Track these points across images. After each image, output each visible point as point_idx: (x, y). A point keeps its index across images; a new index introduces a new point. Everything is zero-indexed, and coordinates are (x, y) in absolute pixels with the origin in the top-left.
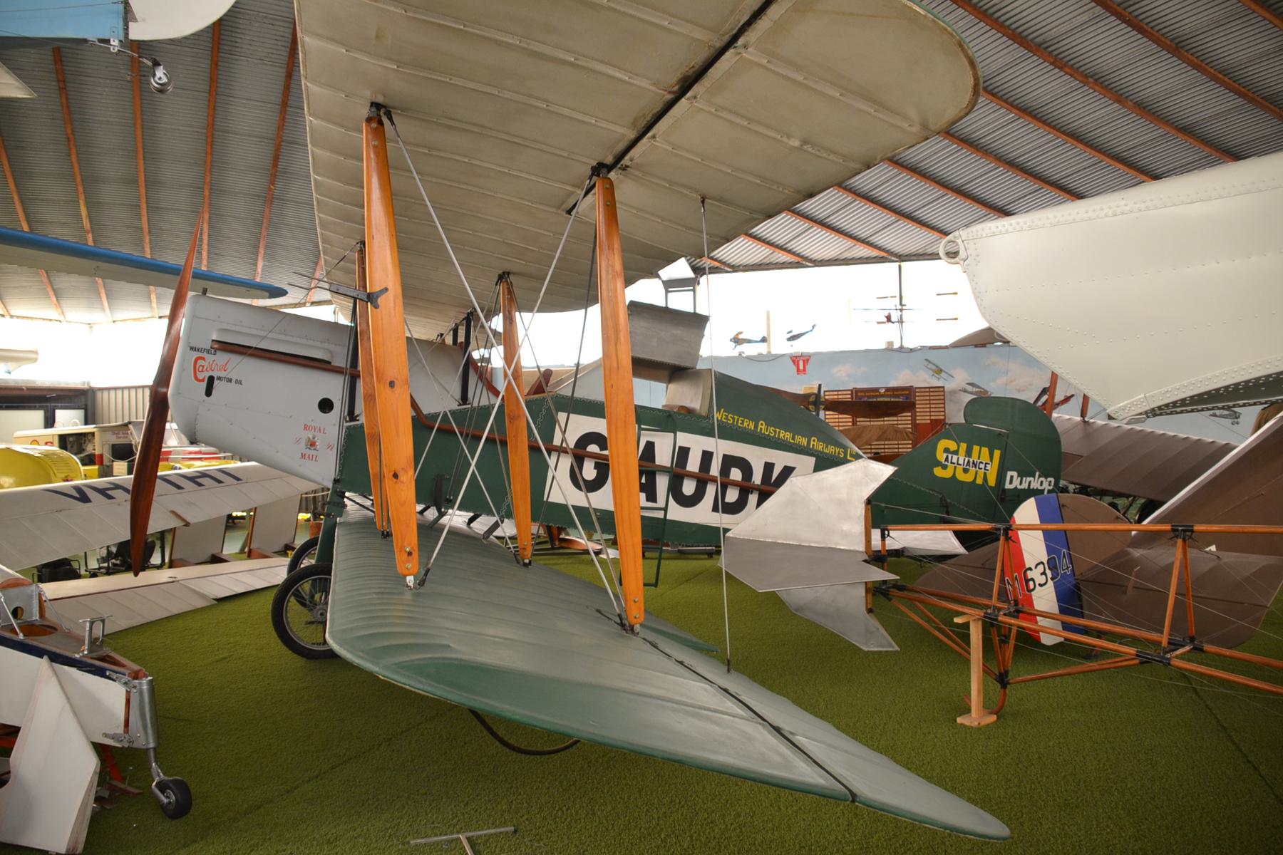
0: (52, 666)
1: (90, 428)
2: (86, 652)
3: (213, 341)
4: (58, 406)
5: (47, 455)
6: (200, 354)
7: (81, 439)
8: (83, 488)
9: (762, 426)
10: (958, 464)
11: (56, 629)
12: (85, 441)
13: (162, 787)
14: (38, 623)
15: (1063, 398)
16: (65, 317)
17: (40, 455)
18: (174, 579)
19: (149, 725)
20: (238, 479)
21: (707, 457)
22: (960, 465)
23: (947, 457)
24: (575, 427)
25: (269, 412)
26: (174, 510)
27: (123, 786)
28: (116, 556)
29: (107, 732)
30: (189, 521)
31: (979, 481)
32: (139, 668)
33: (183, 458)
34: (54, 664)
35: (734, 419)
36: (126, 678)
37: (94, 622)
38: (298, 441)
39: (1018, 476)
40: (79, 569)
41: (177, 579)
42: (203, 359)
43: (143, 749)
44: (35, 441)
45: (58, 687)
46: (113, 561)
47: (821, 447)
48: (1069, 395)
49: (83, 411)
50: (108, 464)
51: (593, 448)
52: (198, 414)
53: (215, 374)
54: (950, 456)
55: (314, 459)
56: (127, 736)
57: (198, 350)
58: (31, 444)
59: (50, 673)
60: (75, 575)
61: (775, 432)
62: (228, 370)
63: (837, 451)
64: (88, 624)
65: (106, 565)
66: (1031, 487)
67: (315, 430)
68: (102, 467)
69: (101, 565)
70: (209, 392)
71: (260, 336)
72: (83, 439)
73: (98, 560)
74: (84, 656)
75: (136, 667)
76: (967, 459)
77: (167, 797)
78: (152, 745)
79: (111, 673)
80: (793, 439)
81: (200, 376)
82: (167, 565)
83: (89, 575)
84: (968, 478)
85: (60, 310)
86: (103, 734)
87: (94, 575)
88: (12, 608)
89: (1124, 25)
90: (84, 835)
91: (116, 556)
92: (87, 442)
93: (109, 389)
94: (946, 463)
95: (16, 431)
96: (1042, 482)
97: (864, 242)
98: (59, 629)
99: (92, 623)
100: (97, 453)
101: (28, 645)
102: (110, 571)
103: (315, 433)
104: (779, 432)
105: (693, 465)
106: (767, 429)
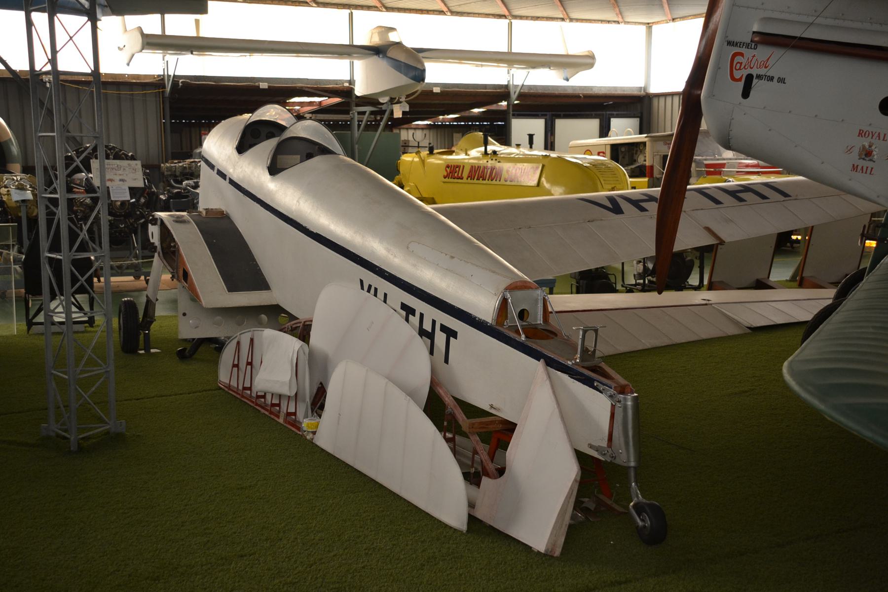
0: (547, 370)
1: (642, 138)
2: (578, 361)
3: (754, 32)
4: (613, 114)
5: (595, 165)
7: (633, 150)
8: (616, 197)
11: (556, 335)
12: (637, 151)
13: (639, 508)
14: (540, 327)
16: (622, 18)
17: (588, 165)
18: (707, 302)
19: (631, 443)
20: (785, 195)
25: (816, 116)
26: (711, 227)
27: (609, 502)
28: (653, 273)
29: (592, 444)
30: (724, 239)
32: (626, 383)
33: (738, 172)
34: (549, 368)
36: (612, 391)
37: (587, 330)
38: (849, 150)
40: (615, 284)
41: (710, 302)
42: (742, 55)
43: (625, 467)
44: (588, 151)
45: (550, 391)
46: (650, 278)
48: (533, 146)
49: (638, 119)
50: (658, 176)
52: (733, 119)
53: (754, 72)
55: (869, 171)
56: (610, 450)
57: (737, 44)
58: (584, 154)
59: (545, 377)
60: (610, 288)
62: (769, 67)
64: (581, 333)
65: (641, 281)
67: (873, 136)
68: (652, 179)
69: (638, 281)
70: (746, 94)
71: (805, 23)
72: (635, 149)
73: (634, 275)
74: (576, 364)
75: (622, 381)
77: (642, 520)
78: (632, 464)
79: (598, 384)
81: (737, 74)
82: (705, 287)
83: (626, 291)
85: (617, 9)
86: (589, 444)
87: (630, 290)
88: (519, 310)
90: (563, 539)
91: (653, 273)
92: (639, 153)
93: (665, 95)
95: (572, 141)
98: (558, 334)
99: (585, 332)
100: (647, 165)
101: (527, 346)
102: (646, 288)
103: (873, 141)
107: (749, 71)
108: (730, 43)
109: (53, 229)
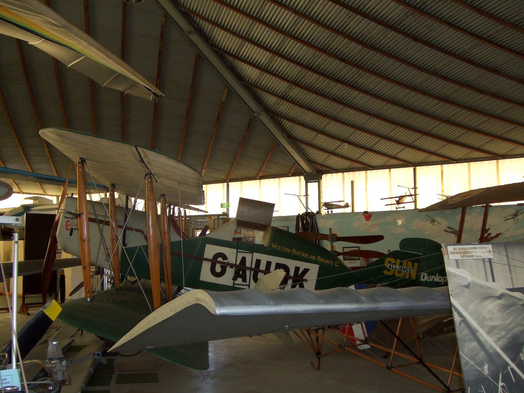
6: (68, 220)
9: (294, 251)
10: (396, 269)
15: (495, 235)
21: (269, 264)
22: (397, 269)
23: (390, 266)
24: (210, 251)
31: (407, 277)
35: (281, 248)
39: (427, 275)
42: (69, 221)
47: (322, 260)
48: (498, 233)
51: (220, 259)
53: (73, 227)
54: (392, 265)
61: (300, 253)
63: (330, 262)
66: (435, 281)
76: (400, 267)
80: (309, 256)
81: (68, 228)
84: (401, 275)
89: (426, 47)
94: (390, 268)
96: (440, 278)
97: (394, 158)
104: (302, 254)
105: (263, 267)
106: (296, 252)
107: (72, 227)
108: (65, 217)
109: (66, 39)
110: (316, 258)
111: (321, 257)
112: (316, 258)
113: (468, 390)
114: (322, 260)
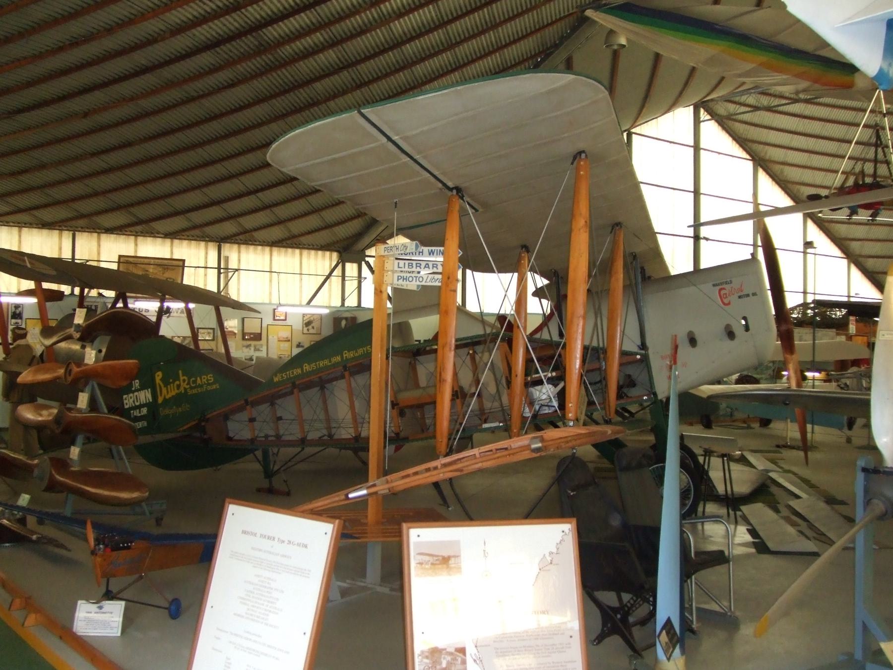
42: (724, 289)
47: (352, 355)
80: (330, 361)
104: (319, 364)
110: (342, 357)
111: (349, 351)
112: (342, 357)
113: (878, 16)
114: (352, 355)
